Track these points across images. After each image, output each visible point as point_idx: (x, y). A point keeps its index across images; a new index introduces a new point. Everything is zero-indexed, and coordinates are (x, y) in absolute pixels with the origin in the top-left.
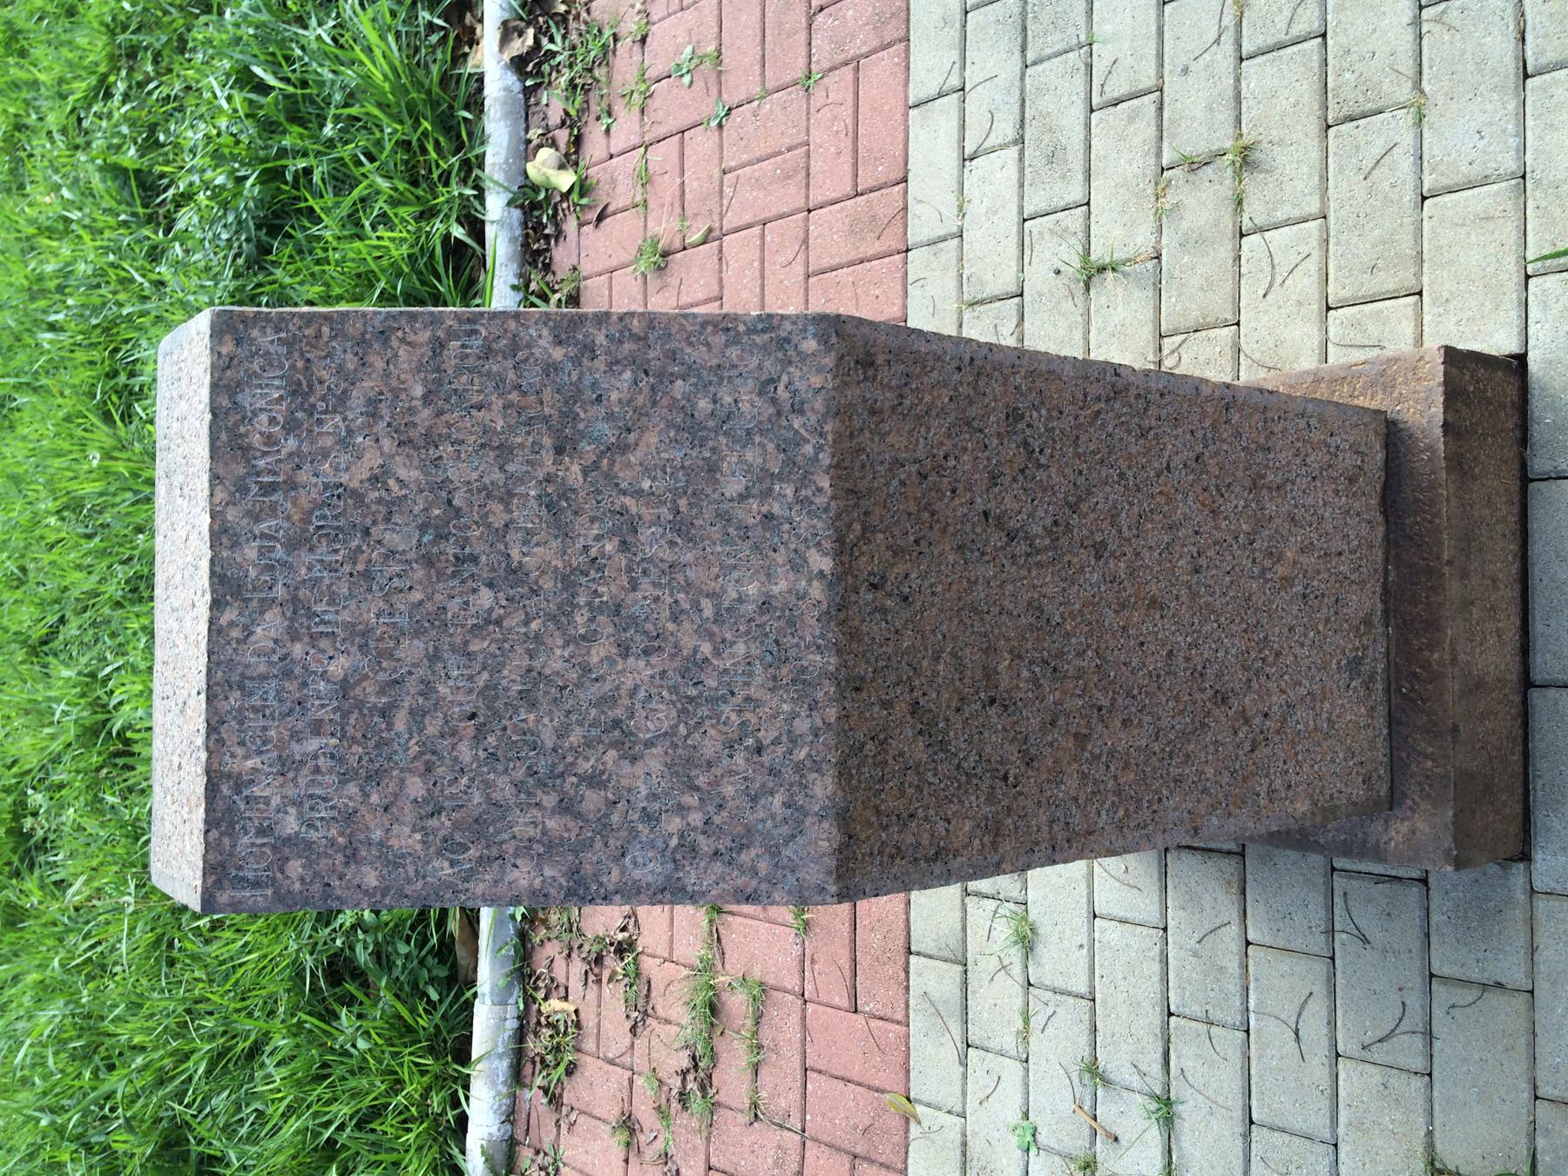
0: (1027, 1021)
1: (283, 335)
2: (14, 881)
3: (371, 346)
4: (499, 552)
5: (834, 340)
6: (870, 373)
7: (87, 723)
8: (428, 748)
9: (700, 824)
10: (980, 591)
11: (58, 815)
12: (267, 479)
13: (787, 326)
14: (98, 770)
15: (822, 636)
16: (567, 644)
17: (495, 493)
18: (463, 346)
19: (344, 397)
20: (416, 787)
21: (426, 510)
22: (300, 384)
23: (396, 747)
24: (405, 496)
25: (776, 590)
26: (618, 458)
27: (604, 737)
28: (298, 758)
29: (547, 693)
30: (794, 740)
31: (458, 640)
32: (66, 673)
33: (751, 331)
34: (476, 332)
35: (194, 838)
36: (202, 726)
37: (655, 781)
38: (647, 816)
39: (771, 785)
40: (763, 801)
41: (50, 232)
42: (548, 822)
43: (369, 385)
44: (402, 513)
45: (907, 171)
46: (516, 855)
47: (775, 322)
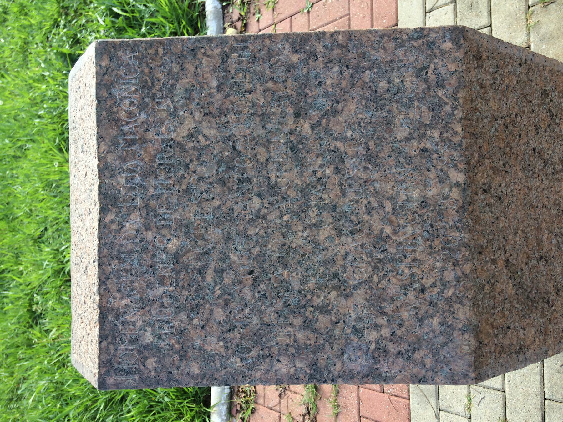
0: (470, 401)
1: (136, 54)
2: (30, 330)
3: (186, 58)
4: (264, 176)
5: (462, 41)
6: (480, 63)
7: (56, 269)
8: (226, 292)
9: (388, 335)
10: (533, 195)
11: (46, 305)
12: (129, 137)
13: (433, 35)
14: (60, 287)
15: (460, 221)
16: (305, 229)
17: (260, 141)
18: (240, 56)
19: (172, 89)
20: (219, 314)
21: (221, 152)
22: (146, 82)
23: (207, 291)
24: (209, 145)
25: (430, 194)
26: (332, 119)
27: (328, 284)
28: (151, 298)
29: (293, 258)
30: (445, 285)
31: (241, 228)
32: (48, 249)
33: (411, 39)
34: (246, 47)
35: (93, 345)
36: (96, 281)
37: (360, 309)
38: (356, 331)
39: (431, 311)
40: (426, 322)
41: (38, 81)
42: (297, 335)
43: (186, 81)
44: (207, 155)
45: (397, 21)
46: (279, 354)
47: (426, 32)
